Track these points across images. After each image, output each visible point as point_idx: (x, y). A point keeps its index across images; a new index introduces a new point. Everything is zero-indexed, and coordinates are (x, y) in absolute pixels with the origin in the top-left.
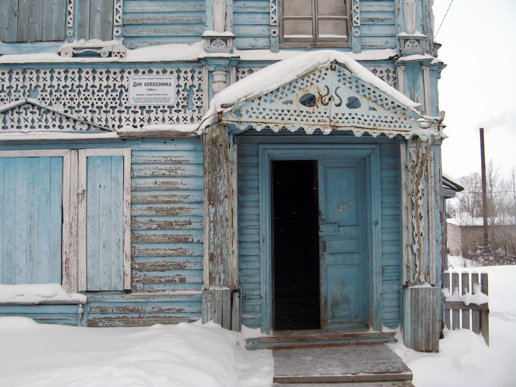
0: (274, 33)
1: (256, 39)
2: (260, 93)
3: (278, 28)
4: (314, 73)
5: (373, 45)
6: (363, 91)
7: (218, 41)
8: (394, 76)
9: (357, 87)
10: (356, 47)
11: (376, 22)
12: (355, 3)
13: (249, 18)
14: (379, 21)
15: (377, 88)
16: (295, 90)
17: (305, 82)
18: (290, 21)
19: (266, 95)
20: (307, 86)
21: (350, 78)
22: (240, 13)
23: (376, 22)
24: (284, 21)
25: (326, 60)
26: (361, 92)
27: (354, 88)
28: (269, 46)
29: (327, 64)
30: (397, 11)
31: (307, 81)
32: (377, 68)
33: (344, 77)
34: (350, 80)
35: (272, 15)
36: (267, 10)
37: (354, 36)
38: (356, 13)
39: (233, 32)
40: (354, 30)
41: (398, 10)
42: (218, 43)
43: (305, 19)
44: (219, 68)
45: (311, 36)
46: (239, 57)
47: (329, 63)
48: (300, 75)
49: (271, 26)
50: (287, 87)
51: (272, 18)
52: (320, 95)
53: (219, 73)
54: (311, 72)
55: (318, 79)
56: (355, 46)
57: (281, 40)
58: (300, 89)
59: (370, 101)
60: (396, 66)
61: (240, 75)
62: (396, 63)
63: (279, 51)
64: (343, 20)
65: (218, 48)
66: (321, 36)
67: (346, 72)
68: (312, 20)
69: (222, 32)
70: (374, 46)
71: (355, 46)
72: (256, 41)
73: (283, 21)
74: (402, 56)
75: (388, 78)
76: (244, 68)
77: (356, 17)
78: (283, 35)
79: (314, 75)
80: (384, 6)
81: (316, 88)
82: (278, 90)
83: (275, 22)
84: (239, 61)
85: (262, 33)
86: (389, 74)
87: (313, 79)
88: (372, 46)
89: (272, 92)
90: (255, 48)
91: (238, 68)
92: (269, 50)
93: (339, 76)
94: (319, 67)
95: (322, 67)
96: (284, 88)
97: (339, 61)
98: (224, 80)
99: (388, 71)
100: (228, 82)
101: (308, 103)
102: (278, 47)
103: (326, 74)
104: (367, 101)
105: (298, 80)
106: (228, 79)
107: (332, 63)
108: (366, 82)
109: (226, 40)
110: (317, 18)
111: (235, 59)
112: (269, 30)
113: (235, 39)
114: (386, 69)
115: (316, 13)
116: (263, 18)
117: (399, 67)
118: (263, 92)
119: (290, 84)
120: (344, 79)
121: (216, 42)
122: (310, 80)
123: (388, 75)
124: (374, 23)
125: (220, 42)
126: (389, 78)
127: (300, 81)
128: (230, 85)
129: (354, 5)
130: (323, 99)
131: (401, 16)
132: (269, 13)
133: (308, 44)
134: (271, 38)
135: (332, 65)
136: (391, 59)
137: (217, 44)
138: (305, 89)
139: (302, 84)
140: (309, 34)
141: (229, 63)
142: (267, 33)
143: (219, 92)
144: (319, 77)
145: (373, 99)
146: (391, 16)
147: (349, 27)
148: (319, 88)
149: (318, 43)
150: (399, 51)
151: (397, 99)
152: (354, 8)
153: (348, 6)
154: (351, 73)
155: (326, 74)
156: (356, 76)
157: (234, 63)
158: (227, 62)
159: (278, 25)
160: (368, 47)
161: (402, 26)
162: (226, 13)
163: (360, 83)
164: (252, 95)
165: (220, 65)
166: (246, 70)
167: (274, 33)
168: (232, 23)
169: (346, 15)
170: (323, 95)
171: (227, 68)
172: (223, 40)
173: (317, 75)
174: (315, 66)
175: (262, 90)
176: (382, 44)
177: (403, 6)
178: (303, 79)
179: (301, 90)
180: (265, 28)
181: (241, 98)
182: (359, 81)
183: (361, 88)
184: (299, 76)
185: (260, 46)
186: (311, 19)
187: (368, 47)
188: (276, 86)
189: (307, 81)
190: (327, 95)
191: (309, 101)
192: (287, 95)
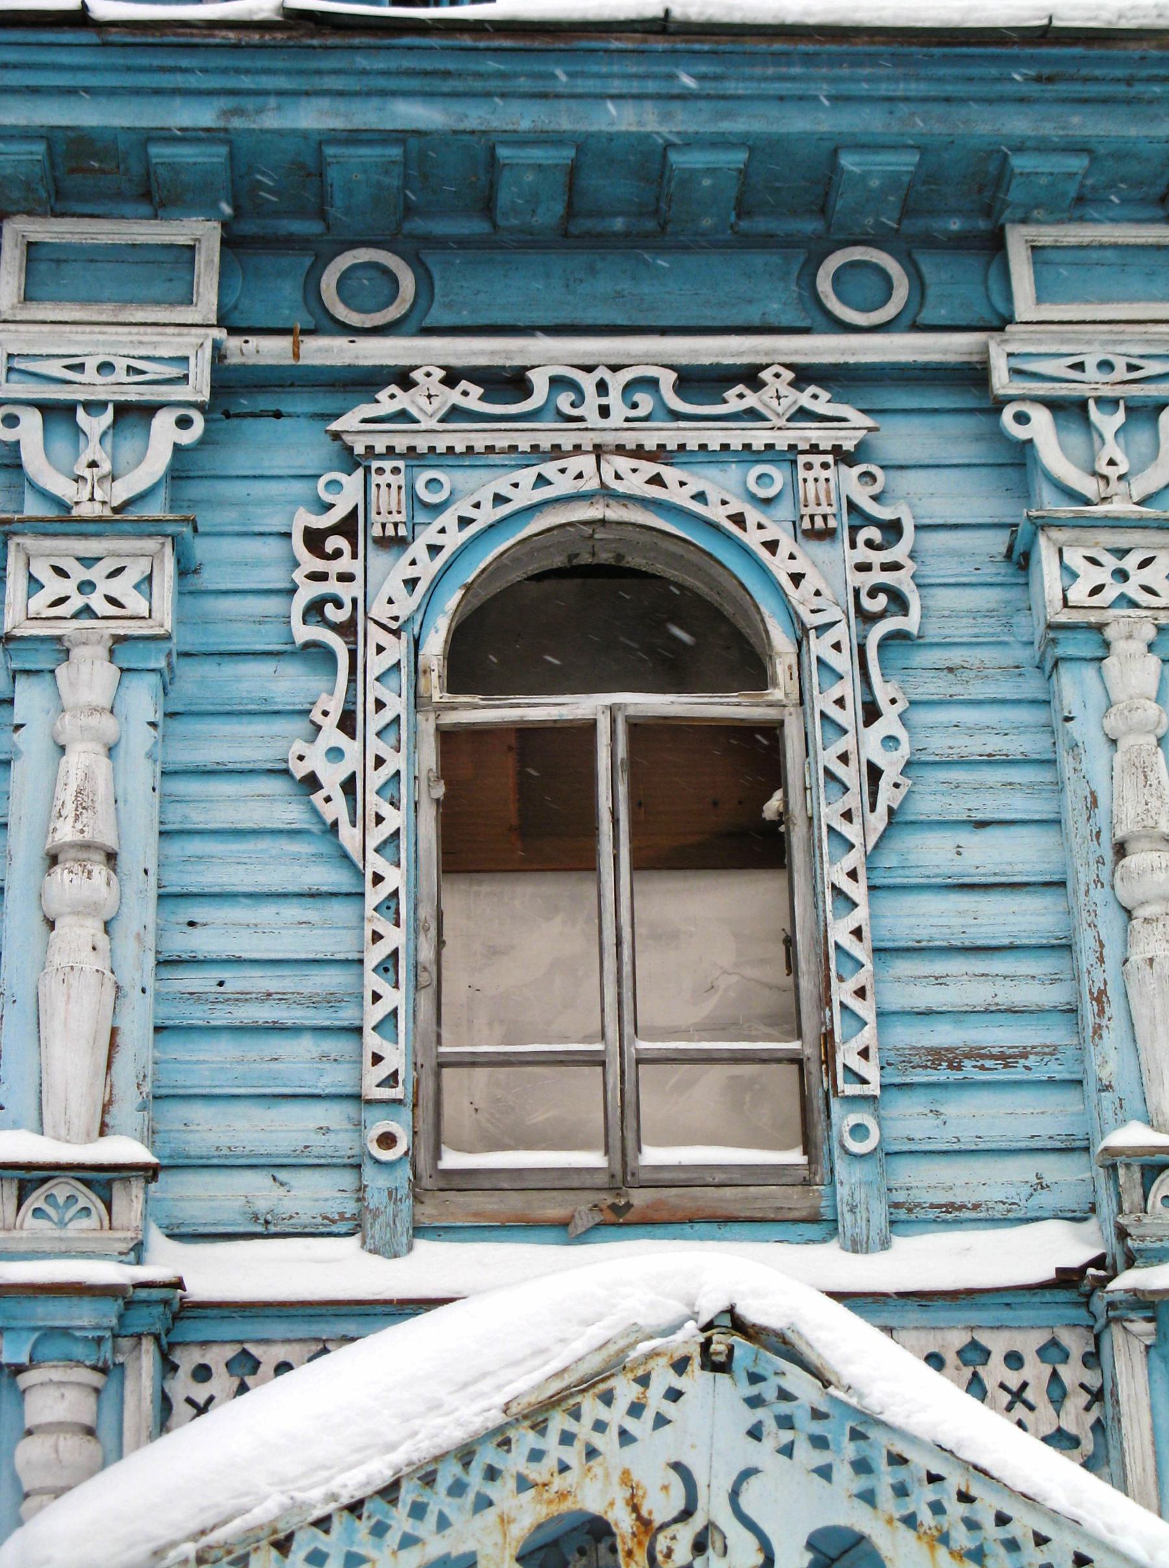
0: (387, 1140)
1: (282, 1175)
2: (286, 1511)
3: (406, 1113)
4: (602, 1387)
5: (958, 1201)
6: (901, 1491)
7: (61, 1190)
8: (1092, 1379)
9: (862, 1466)
10: (862, 1213)
11: (969, 1070)
12: (850, 965)
13: (241, 1062)
14: (989, 1063)
15: (985, 1473)
16: (492, 1491)
17: (551, 1442)
18: (481, 1073)
19: (323, 1523)
20: (564, 1468)
21: (817, 1415)
22: (191, 1029)
23: (969, 1070)
24: (446, 1072)
25: (675, 1309)
26: (885, 1495)
27: (843, 1473)
28: (353, 1217)
29: (679, 1337)
30: (1089, 1009)
31: (567, 1438)
32: (984, 1338)
33: (784, 1408)
34: (817, 1428)
35: (373, 1041)
36: (346, 1016)
37: (847, 1152)
38: (854, 1024)
39: (151, 1137)
40: (845, 1119)
41: (1099, 1000)
42: (61, 1200)
43: (562, 1063)
44: (59, 1346)
45: (594, 1159)
46: (179, 1284)
47: (691, 1327)
48: (524, 1401)
49: (369, 1102)
50: (449, 1473)
51: (377, 1059)
52: (639, 1518)
53: (57, 1375)
54: (587, 1384)
55: (631, 1425)
56: (852, 1210)
57: (427, 1182)
58: (523, 1484)
59: (942, 1552)
60: (1102, 1321)
61: (182, 1386)
62: (1099, 1303)
63: (410, 1248)
64: (779, 1061)
65: (57, 1233)
66: (653, 1155)
67: (796, 1380)
68: (603, 1064)
69: (88, 1139)
70: (962, 1207)
71: (852, 1210)
72: (282, 1191)
73: (438, 1076)
74: (1130, 1263)
75: (1057, 1394)
76: (205, 1343)
77: (858, 1043)
78: (437, 1156)
79: (607, 1399)
80: (1012, 978)
81: (616, 1478)
82: (390, 1492)
83: (392, 1079)
84: (176, 1305)
85: (317, 1140)
86: (1062, 1370)
87: (600, 1426)
88: (950, 1207)
89: (355, 1508)
90: (272, 1229)
91: (172, 1345)
92: (353, 1242)
93: (755, 1402)
94: (633, 1355)
95: (654, 1354)
96: (429, 1480)
97: (753, 1312)
98: (88, 1419)
99: (1054, 1351)
100: (106, 1431)
101: (582, 1552)
102: (404, 1224)
103: (674, 1395)
104: (925, 1548)
105: (512, 1434)
106: (108, 1420)
107: (709, 1326)
108: (912, 1440)
109: (109, 1184)
110: (631, 1053)
111: (156, 1294)
112: (359, 1126)
113: (162, 1176)
114: (1039, 1338)
115: (628, 1029)
116: (324, 1057)
117: (1115, 1329)
118: (300, 1507)
119: (465, 1454)
120: (786, 1422)
121: (50, 1198)
122: (583, 1430)
123: (1055, 1374)
124: (959, 1075)
125: (71, 1199)
126: (1064, 1394)
127: (526, 1439)
128: (120, 1456)
129: (841, 979)
130: (662, 1543)
131: (1113, 1035)
132: (359, 1030)
133: (580, 1207)
134: (368, 1171)
135: (708, 1342)
136: (1067, 1279)
137: (55, 1205)
138: (555, 1487)
139: (536, 1455)
140: (584, 1145)
141: (121, 1317)
142: (342, 1143)
143: (58, 1493)
144: (636, 1409)
145: (962, 1538)
146: (1056, 1034)
147: (818, 1103)
148: (636, 1476)
149: (639, 1198)
150: (1110, 1230)
151: (1108, 1537)
152: (842, 992)
153: (808, 985)
154: (826, 1384)
155: (674, 1395)
156: (853, 1401)
157: (148, 1319)
158: (108, 1313)
159: (409, 1100)
160: (932, 1214)
161: (1125, 1086)
162: (114, 1032)
163: (881, 1441)
164: (237, 1525)
165: (65, 1332)
166: (217, 1357)
167: (387, 1140)
168: (147, 1088)
169: (800, 1036)
170: (658, 1519)
171: (108, 1346)
172: (87, 1183)
173: (622, 1402)
174: (612, 1349)
175: (300, 1496)
176: (1011, 1193)
177: (1125, 977)
178: (540, 1428)
179: (531, 1493)
180: (334, 1115)
181: (173, 1544)
182: (873, 1433)
183: (886, 1477)
184: (514, 1409)
185: (304, 1219)
186: (597, 1061)
187: (932, 1214)
188: (379, 1470)
189: (567, 1438)
190: (686, 1514)
191: (584, 1539)
192: (443, 1523)
